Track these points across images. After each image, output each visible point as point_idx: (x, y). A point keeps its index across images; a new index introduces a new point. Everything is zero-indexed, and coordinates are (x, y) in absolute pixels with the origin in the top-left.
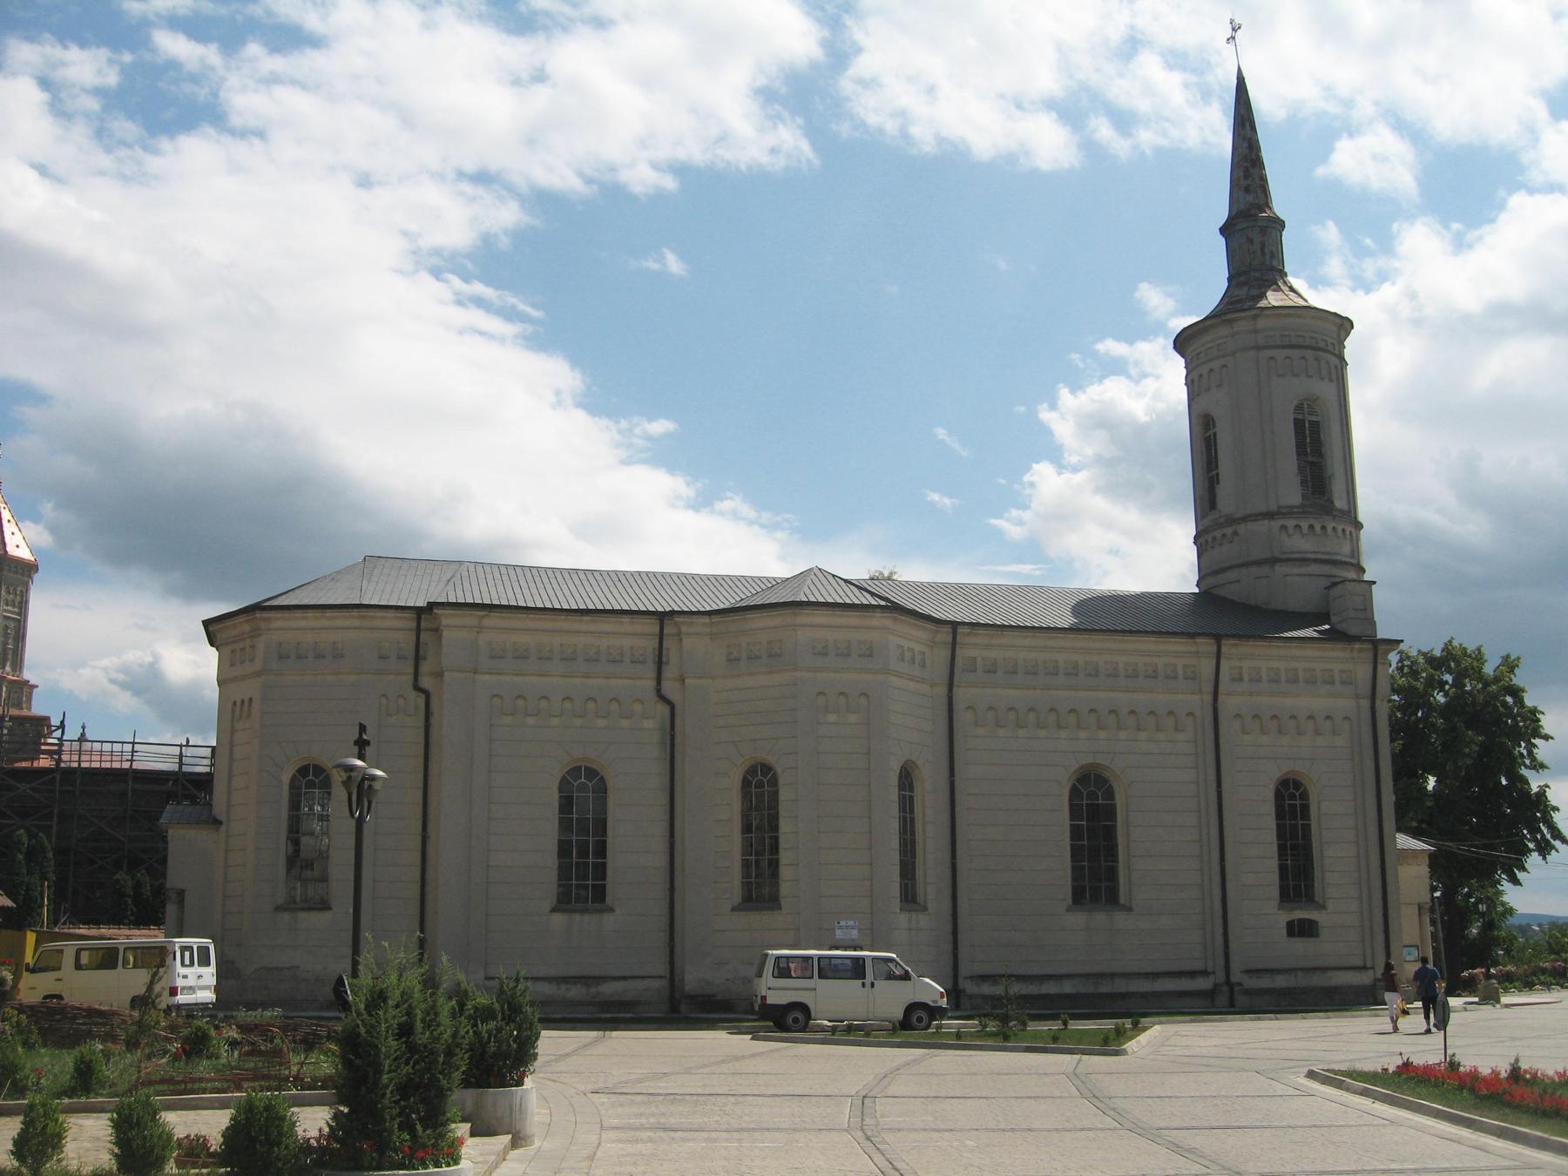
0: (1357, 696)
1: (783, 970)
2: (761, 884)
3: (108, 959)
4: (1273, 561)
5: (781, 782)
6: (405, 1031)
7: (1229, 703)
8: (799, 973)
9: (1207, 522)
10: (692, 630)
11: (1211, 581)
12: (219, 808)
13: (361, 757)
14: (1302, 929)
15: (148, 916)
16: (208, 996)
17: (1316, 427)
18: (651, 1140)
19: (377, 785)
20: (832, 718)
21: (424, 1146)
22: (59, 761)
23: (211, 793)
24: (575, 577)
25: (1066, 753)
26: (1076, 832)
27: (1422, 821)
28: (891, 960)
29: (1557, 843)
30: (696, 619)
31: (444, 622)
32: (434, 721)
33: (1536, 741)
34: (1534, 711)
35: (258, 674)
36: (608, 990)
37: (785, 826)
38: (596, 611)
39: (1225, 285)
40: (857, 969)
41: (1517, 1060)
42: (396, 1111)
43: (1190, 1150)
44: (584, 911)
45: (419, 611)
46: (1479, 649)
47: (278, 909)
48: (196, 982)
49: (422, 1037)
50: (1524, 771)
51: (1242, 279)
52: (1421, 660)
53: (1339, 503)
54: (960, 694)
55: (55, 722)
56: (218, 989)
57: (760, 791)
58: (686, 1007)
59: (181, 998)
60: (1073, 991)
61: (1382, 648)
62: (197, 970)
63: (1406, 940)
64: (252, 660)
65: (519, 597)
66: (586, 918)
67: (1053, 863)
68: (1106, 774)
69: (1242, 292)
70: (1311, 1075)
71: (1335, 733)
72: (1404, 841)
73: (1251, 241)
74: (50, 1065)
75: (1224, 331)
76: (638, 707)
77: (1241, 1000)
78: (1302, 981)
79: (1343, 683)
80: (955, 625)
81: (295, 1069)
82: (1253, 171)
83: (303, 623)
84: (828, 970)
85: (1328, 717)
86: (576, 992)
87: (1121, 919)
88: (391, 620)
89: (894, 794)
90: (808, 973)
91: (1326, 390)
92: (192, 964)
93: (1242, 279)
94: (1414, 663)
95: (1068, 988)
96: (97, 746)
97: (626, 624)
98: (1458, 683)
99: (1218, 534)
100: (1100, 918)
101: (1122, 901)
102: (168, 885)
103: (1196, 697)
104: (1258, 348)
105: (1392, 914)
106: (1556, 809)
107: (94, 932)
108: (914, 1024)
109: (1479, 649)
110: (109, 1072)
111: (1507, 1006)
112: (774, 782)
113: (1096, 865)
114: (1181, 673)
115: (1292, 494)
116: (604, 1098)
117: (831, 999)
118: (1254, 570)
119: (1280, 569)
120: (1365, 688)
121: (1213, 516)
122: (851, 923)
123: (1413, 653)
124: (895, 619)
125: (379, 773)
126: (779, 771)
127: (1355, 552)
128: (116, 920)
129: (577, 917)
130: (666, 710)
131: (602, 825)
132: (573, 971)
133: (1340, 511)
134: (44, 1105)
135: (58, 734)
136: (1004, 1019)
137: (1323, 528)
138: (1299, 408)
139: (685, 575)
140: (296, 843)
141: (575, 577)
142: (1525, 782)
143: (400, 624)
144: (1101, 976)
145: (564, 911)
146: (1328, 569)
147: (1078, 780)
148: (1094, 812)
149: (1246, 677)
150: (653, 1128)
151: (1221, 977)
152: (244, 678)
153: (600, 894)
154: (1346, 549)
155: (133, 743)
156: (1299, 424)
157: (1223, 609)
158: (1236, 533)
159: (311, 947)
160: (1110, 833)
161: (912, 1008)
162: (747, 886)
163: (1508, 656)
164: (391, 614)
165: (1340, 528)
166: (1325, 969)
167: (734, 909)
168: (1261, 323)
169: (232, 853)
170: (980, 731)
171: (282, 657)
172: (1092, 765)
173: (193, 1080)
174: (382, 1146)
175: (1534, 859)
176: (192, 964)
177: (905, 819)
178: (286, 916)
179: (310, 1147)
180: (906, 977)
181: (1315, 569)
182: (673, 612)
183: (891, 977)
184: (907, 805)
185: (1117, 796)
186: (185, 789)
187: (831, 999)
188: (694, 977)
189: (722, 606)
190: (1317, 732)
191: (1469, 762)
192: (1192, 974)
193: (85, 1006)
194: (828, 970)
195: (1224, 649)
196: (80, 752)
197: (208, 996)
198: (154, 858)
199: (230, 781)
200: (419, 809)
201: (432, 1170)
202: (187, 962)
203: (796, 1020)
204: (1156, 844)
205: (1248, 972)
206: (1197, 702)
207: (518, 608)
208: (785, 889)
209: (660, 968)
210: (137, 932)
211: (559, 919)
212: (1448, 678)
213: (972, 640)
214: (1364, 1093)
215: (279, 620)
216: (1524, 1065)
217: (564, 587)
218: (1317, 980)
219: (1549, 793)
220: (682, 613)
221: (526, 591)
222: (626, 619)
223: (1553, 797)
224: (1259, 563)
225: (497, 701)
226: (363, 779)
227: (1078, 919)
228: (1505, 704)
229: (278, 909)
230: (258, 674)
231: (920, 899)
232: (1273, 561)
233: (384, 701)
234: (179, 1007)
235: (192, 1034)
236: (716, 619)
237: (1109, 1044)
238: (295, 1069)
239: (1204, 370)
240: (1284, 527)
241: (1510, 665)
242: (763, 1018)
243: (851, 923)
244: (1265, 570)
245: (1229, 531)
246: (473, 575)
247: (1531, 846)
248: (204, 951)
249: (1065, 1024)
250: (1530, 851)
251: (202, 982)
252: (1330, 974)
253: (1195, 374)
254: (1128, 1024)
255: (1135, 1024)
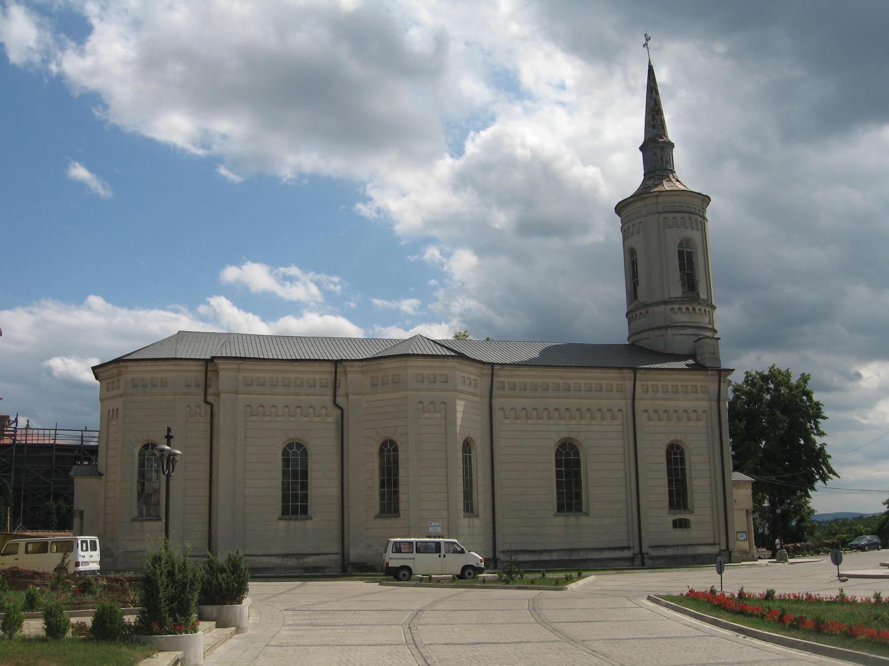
0: (710, 400)
1: (398, 548)
2: (390, 505)
3: (43, 548)
4: (667, 327)
5: (400, 449)
6: (171, 574)
7: (640, 405)
8: (406, 550)
9: (632, 306)
10: (352, 369)
11: (635, 338)
12: (101, 467)
13: (169, 445)
14: (681, 524)
15: (64, 524)
16: (96, 566)
17: (690, 254)
18: (304, 630)
19: (177, 458)
20: (426, 415)
21: (180, 625)
22: (15, 440)
23: (97, 456)
24: (291, 341)
25: (553, 432)
26: (559, 474)
27: (757, 464)
28: (455, 543)
29: (831, 475)
30: (353, 363)
31: (220, 367)
32: (215, 419)
33: (819, 420)
34: (817, 404)
35: (121, 396)
36: (310, 561)
37: (402, 472)
38: (301, 360)
39: (641, 178)
40: (437, 548)
41: (742, 589)
42: (168, 608)
43: (559, 632)
44: (296, 519)
45: (207, 361)
46: (787, 371)
47: (133, 520)
48: (89, 560)
49: (178, 576)
50: (813, 436)
51: (651, 175)
52: (758, 376)
53: (703, 295)
54: (496, 402)
55: (13, 418)
56: (101, 563)
57: (389, 453)
58: (349, 568)
59: (81, 568)
60: (557, 558)
61: (723, 373)
62: (90, 553)
63: (737, 529)
64: (118, 388)
65: (260, 353)
66: (297, 523)
67: (549, 493)
68: (575, 443)
69: (650, 183)
70: (649, 598)
71: (698, 419)
72: (738, 476)
73: (656, 155)
74: (15, 598)
75: (640, 204)
76: (324, 411)
77: (648, 562)
78: (681, 551)
79: (702, 392)
80: (492, 365)
81: (132, 597)
82: (657, 117)
83: (145, 368)
84: (422, 549)
85: (695, 411)
86: (292, 562)
87: (584, 520)
88: (192, 367)
89: (460, 455)
90: (410, 550)
91: (696, 236)
92: (87, 550)
93: (651, 175)
94: (754, 378)
95: (555, 557)
96: (36, 432)
97: (317, 367)
98: (777, 389)
99: (638, 313)
100: (572, 519)
101: (584, 510)
102: (75, 508)
103: (623, 402)
104: (659, 213)
105: (729, 515)
106: (829, 457)
107: (35, 534)
108: (467, 576)
109: (787, 371)
110: (43, 600)
111: (792, 563)
112: (396, 450)
113: (570, 493)
114: (615, 389)
115: (677, 290)
116: (290, 613)
117: (421, 563)
118: (657, 332)
119: (671, 332)
120: (716, 397)
121: (636, 303)
122: (437, 524)
123: (754, 373)
124: (460, 362)
125: (179, 452)
126: (399, 444)
127: (711, 322)
128: (47, 527)
129: (292, 523)
130: (339, 412)
131: (305, 473)
132: (291, 551)
133: (704, 300)
134: (14, 608)
135: (14, 425)
136: (509, 573)
137: (694, 309)
138: (681, 244)
139: (350, 339)
140: (143, 485)
141: (291, 341)
142: (815, 443)
143: (197, 368)
144: (572, 550)
145: (285, 519)
146: (696, 331)
147: (560, 446)
148: (295, 465)
149: (650, 390)
150: (308, 625)
151: (637, 550)
152: (114, 397)
153: (305, 510)
154: (707, 320)
155: (56, 430)
156: (681, 254)
157: (638, 353)
158: (647, 312)
159: (149, 541)
160: (578, 474)
161: (466, 568)
162: (382, 505)
163: (804, 374)
164: (192, 363)
165: (703, 309)
166: (693, 545)
167: (376, 517)
168: (660, 199)
169: (109, 489)
170: (507, 421)
171: (135, 386)
172: (568, 438)
173: (83, 603)
174: (161, 625)
175: (819, 484)
176: (87, 550)
177: (466, 468)
178: (138, 524)
179: (131, 625)
180: (462, 552)
181: (689, 331)
182: (342, 360)
183: (455, 551)
184: (467, 461)
185: (581, 455)
186: (83, 455)
187: (421, 563)
188: (355, 553)
189: (369, 356)
190: (689, 419)
191: (782, 432)
192: (622, 549)
193: (31, 569)
194: (422, 549)
195: (637, 376)
196: (26, 435)
197: (96, 566)
198: (66, 494)
199: (107, 452)
200: (208, 466)
201: (184, 634)
202: (84, 548)
203: (404, 575)
204: (602, 479)
205: (651, 547)
206: (624, 404)
207: (259, 359)
208: (402, 506)
209: (335, 548)
210: (58, 533)
211: (282, 524)
212: (772, 386)
213: (502, 373)
214: (667, 606)
215: (132, 367)
216: (745, 591)
217: (285, 346)
218: (690, 551)
219: (826, 448)
220: (347, 360)
221: (264, 349)
222: (317, 364)
223: (828, 450)
224: (660, 328)
225: (248, 408)
226: (169, 455)
227: (560, 520)
228: (802, 401)
229: (133, 520)
230: (121, 396)
231: (689, 506)
232: (667, 327)
233: (188, 409)
234: (80, 572)
235: (85, 583)
236: (364, 363)
237: (558, 585)
238: (132, 597)
239: (630, 224)
240: (672, 309)
241: (805, 379)
242: (387, 574)
243: (437, 524)
244: (662, 332)
245: (643, 311)
246: (236, 340)
247: (817, 477)
248: (93, 543)
249: (544, 575)
250: (817, 480)
251: (92, 559)
252: (696, 548)
253: (625, 227)
254: (575, 574)
255: (579, 575)
